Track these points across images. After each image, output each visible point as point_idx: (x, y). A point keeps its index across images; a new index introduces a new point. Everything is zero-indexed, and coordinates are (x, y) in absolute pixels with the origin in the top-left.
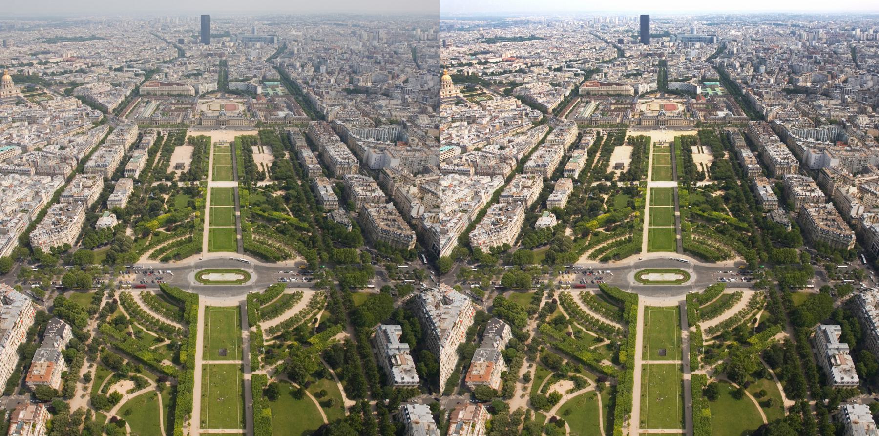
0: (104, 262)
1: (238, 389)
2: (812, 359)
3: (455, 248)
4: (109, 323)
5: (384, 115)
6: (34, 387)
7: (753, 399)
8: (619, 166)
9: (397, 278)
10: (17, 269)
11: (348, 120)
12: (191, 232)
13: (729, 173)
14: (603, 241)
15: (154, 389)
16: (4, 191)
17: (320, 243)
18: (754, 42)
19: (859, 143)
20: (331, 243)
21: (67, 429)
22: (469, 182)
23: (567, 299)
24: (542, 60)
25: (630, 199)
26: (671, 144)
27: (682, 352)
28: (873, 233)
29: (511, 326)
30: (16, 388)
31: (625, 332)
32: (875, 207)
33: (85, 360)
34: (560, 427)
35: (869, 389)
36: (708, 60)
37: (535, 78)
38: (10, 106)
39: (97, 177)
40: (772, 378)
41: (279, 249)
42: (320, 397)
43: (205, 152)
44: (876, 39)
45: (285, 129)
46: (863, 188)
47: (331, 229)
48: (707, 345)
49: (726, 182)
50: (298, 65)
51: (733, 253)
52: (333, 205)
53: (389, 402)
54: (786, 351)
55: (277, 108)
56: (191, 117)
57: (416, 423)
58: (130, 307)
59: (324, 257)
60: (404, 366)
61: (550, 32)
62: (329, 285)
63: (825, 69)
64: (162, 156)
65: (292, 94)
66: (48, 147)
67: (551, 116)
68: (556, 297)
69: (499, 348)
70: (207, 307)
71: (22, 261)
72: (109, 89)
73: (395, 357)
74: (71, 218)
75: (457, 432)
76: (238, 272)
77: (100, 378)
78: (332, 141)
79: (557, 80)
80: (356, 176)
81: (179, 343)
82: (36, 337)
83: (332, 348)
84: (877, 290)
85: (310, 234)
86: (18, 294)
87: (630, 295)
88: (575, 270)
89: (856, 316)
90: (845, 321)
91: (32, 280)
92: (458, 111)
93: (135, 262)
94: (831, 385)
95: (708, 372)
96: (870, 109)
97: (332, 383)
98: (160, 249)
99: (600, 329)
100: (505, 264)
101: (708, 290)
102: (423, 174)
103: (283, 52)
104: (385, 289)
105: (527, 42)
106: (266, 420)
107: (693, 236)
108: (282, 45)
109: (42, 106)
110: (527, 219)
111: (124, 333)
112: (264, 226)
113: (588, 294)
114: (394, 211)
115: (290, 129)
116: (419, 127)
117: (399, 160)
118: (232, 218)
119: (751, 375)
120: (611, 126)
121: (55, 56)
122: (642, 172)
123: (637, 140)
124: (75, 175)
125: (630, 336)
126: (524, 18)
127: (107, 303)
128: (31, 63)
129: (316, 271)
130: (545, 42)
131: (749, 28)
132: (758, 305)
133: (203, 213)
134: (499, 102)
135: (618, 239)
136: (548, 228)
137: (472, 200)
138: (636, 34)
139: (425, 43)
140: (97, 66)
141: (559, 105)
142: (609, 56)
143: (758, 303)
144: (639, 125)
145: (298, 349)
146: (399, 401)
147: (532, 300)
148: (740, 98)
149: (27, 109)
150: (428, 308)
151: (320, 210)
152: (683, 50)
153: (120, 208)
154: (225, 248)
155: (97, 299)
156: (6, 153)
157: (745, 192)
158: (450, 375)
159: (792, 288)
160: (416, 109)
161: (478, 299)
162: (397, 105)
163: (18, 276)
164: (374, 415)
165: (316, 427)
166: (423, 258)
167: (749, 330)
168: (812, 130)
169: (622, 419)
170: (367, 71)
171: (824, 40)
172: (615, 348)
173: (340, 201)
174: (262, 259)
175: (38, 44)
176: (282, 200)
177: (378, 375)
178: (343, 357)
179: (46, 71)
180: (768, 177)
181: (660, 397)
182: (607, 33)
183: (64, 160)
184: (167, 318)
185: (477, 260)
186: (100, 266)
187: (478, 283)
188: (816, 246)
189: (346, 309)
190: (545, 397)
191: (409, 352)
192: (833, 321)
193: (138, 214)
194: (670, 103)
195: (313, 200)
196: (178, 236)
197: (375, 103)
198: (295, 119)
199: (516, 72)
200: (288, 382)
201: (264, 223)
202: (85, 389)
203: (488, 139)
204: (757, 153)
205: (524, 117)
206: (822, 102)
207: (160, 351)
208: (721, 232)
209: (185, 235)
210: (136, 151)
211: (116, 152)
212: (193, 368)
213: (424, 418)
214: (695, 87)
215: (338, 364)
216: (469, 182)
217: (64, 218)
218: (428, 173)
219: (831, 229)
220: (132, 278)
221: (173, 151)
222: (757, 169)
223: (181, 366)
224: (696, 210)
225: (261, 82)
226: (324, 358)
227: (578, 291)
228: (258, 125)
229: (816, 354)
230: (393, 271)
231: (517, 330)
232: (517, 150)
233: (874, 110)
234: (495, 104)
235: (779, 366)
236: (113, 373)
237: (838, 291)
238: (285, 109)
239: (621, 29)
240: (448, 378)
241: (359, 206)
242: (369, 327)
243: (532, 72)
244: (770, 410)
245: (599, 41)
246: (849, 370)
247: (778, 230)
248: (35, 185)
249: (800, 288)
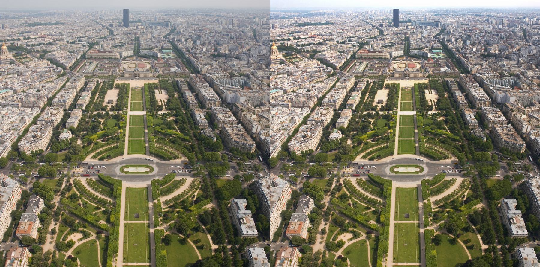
0: (64, 160)
1: (146, 238)
2: (499, 220)
3: (279, 152)
4: (67, 198)
5: (236, 71)
6: (21, 237)
7: (462, 244)
8: (380, 102)
9: (244, 170)
10: (10, 165)
11: (214, 74)
12: (117, 142)
13: (448, 106)
14: (370, 147)
15: (95, 238)
16: (2, 117)
17: (196, 149)
18: (463, 26)
19: (528, 88)
20: (203, 149)
21: (41, 263)
22: (288, 111)
23: (348, 183)
24: (333, 37)
25: (387, 122)
26: (412, 88)
27: (419, 216)
28: (537, 143)
29: (314, 200)
30: (10, 237)
31: (384, 203)
32: (538, 127)
33: (52, 221)
34: (344, 261)
35: (534, 238)
36: (435, 37)
37: (329, 48)
38: (6, 65)
39: (60, 109)
40: (474, 232)
41: (171, 152)
42: (197, 243)
43: (126, 93)
44: (538, 24)
45: (175, 79)
46: (530, 115)
47: (203, 140)
48: (435, 212)
49: (446, 111)
50: (183, 40)
51: (450, 155)
52: (205, 125)
53: (239, 246)
54: (483, 215)
55: (170, 66)
56: (117, 71)
57: (256, 259)
58: (80, 188)
59: (199, 157)
60: (248, 224)
61: (338, 19)
62: (202, 174)
63: (507, 42)
64: (100, 95)
65: (180, 57)
66: (29, 90)
67: (339, 71)
68: (342, 182)
69: (307, 213)
70: (127, 188)
71: (14, 160)
72: (67, 54)
73: (243, 219)
74: (44, 133)
75: (281, 264)
76: (146, 166)
77: (61, 231)
78: (204, 86)
79: (342, 49)
80: (219, 108)
81: (110, 210)
82: (22, 207)
83: (204, 213)
84: (539, 178)
85: (191, 143)
86: (11, 180)
87: (387, 181)
88: (353, 165)
89: (526, 194)
90: (519, 197)
91: (19, 172)
92: (281, 68)
93: (83, 161)
94: (511, 236)
95: (435, 228)
96: (534, 67)
97: (204, 234)
98: (98, 152)
99: (369, 201)
100: (310, 162)
101: (435, 177)
102: (260, 106)
103: (174, 32)
104: (236, 177)
105: (324, 26)
106: (163, 257)
107: (426, 145)
108: (173, 28)
109: (26, 65)
110: (324, 134)
111: (76, 204)
112: (162, 139)
113: (361, 180)
114: (242, 130)
115: (178, 79)
116: (257, 78)
117: (245, 98)
118: (143, 133)
119: (461, 230)
120: (376, 77)
121: (34, 34)
122: (394, 105)
123: (392, 86)
124: (46, 107)
125: (387, 206)
126: (322, 11)
127: (66, 186)
128: (19, 39)
129: (194, 166)
130: (335, 26)
131: (460, 17)
132: (466, 187)
133: (125, 131)
134: (307, 63)
135: (380, 146)
136: (337, 140)
137: (290, 122)
138: (391, 21)
139: (261, 26)
140: (60, 40)
141: (344, 64)
142: (374, 35)
143: (465, 185)
144: (392, 76)
145: (183, 214)
146: (245, 246)
147: (327, 184)
148: (455, 60)
149: (16, 67)
150: (263, 189)
151: (197, 128)
152: (420, 31)
153: (73, 128)
154: (138, 152)
155: (60, 183)
156: (4, 94)
157: (458, 118)
158: (276, 230)
159: (486, 176)
160: (256, 67)
161: (294, 183)
162: (244, 64)
163: (11, 169)
164: (230, 254)
165: (194, 261)
166: (260, 158)
167: (460, 202)
168: (499, 80)
169: (382, 257)
170: (226, 44)
171: (506, 25)
172: (378, 213)
173: (209, 123)
174: (161, 158)
175: (23, 27)
176: (173, 123)
177: (232, 230)
178: (211, 219)
179: (28, 43)
180: (472, 108)
181: (406, 243)
182: (373, 20)
183: (39, 98)
184: (103, 195)
185: (293, 159)
186: (61, 163)
187: (294, 174)
188: (501, 150)
189: (212, 189)
190: (335, 243)
191: (251, 216)
192: (512, 196)
193: (85, 131)
194: (412, 63)
195: (192, 122)
196: (109, 145)
197: (230, 63)
198: (181, 73)
199: (317, 44)
200: (177, 234)
201: (162, 137)
202: (52, 238)
203: (300, 85)
204: (465, 94)
205: (322, 72)
206: (505, 63)
207: (98, 215)
208: (443, 142)
209: (113, 144)
210: (84, 93)
211: (71, 93)
212: (118, 225)
213: (261, 256)
214: (427, 53)
215: (207, 223)
216: (288, 111)
217: (39, 134)
218: (263, 106)
219: (510, 140)
220: (81, 170)
221: (106, 92)
222: (465, 103)
223: (111, 224)
224: (428, 129)
225: (161, 50)
226: (199, 219)
227: (355, 178)
228: (159, 77)
229: (501, 217)
230: (242, 166)
231: (317, 202)
232: (318, 92)
233: (537, 67)
234: (304, 64)
235: (479, 224)
236: (69, 229)
237: (515, 178)
238: (175, 67)
239: (381, 18)
240: (275, 231)
241: (221, 126)
242: (226, 200)
243: (327, 44)
244: (473, 251)
245: (368, 25)
246: (521, 227)
247: (478, 141)
248: (21, 113)
249: (491, 176)
